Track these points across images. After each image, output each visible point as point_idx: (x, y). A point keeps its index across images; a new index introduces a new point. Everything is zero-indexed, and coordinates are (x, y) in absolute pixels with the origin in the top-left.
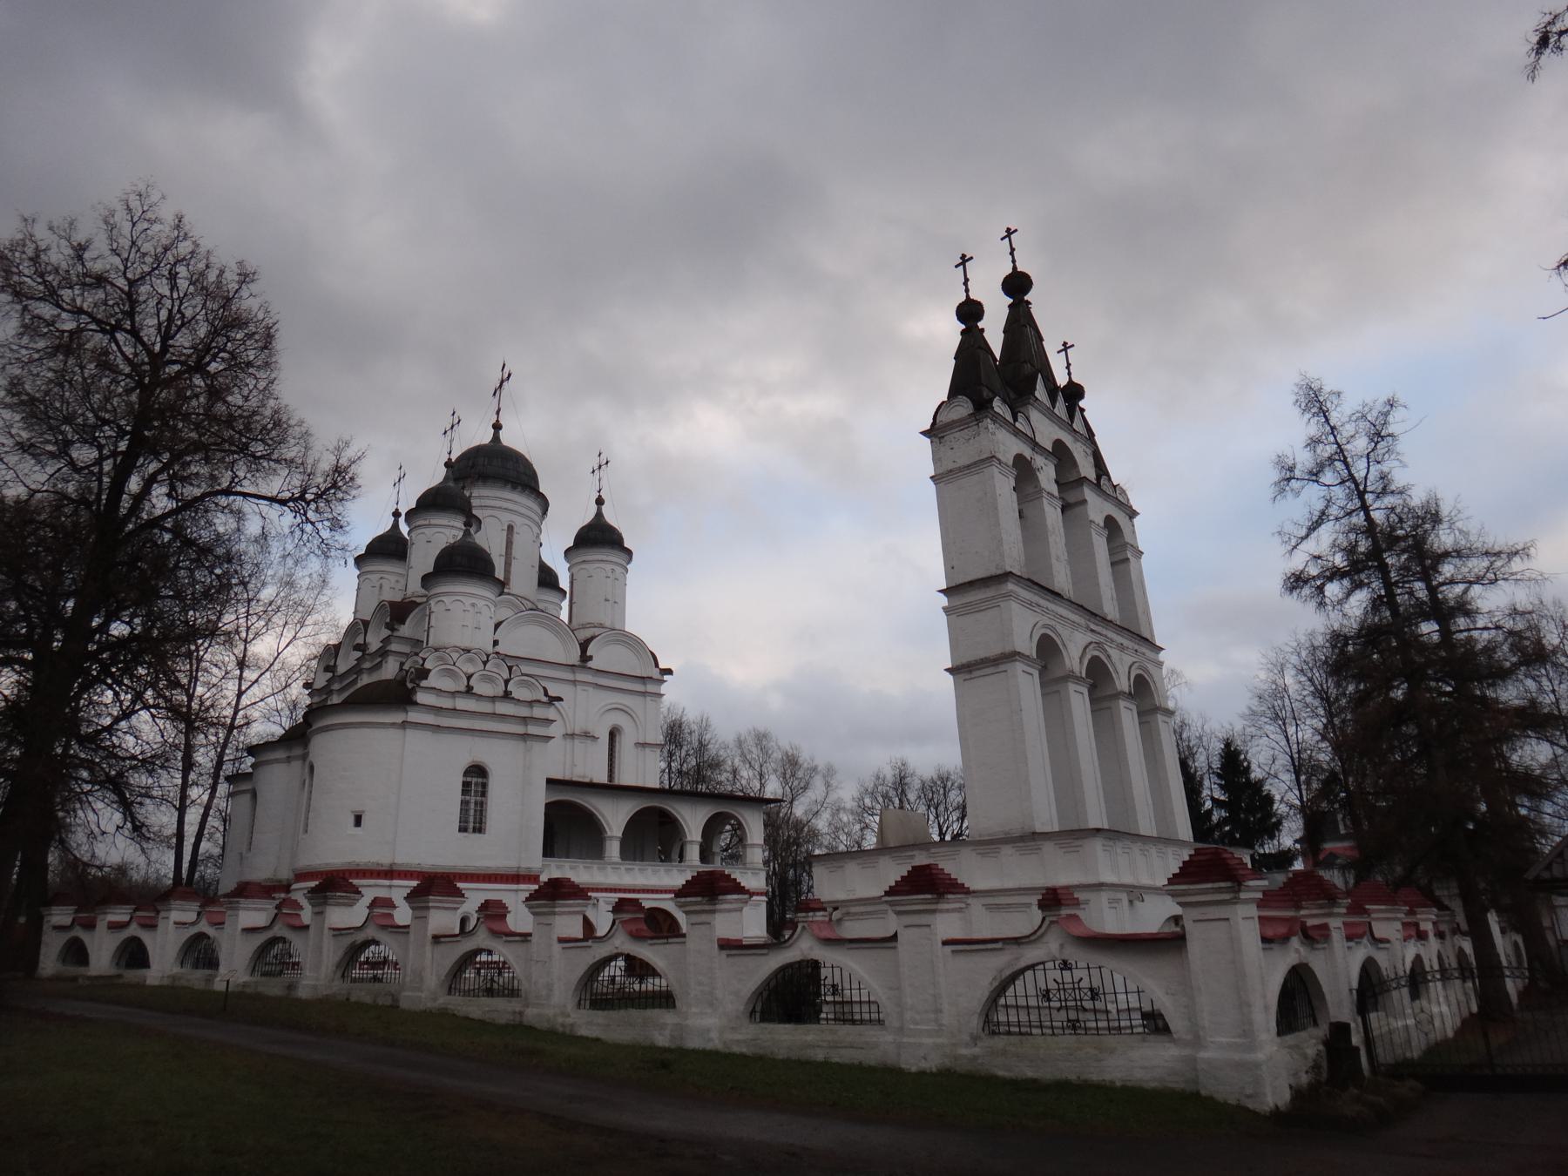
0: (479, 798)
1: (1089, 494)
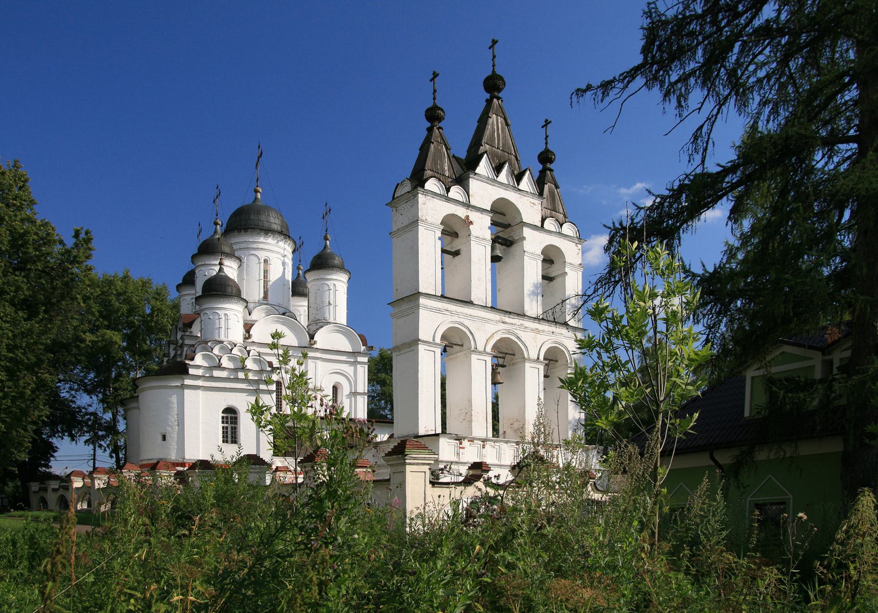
0: (233, 425)
1: (527, 232)
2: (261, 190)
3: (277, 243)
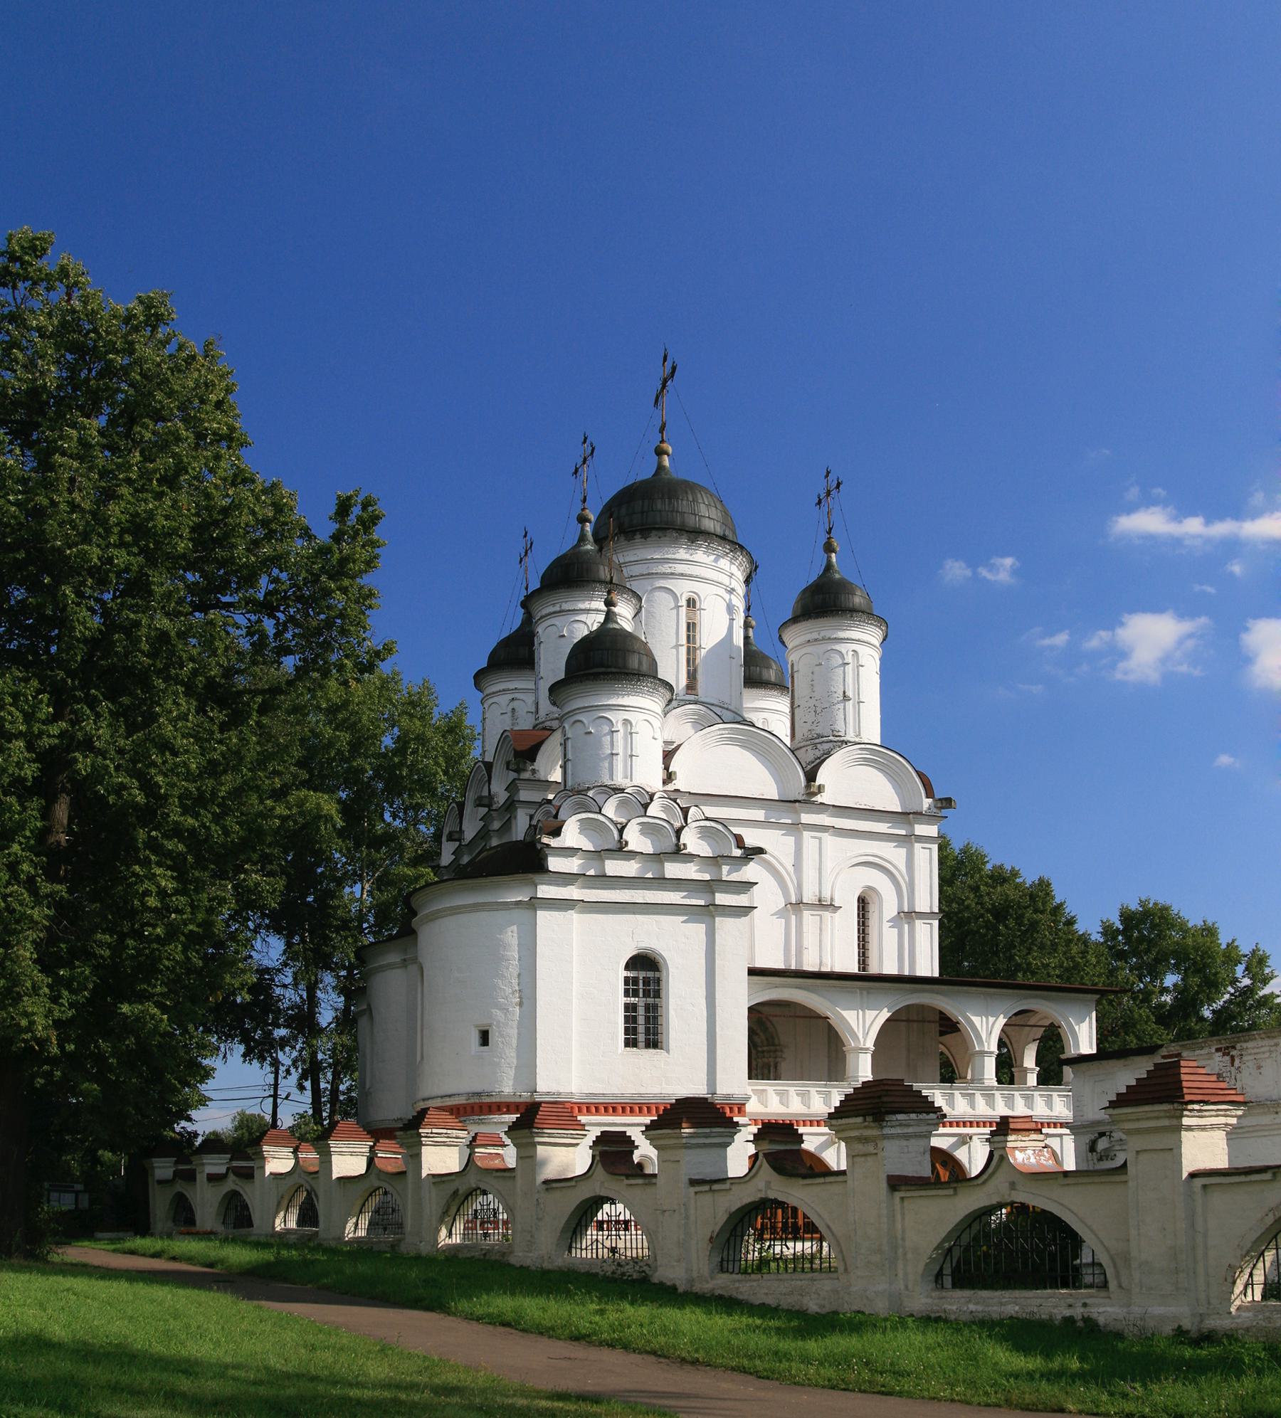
0: (650, 1000)
2: (670, 450)
3: (716, 561)
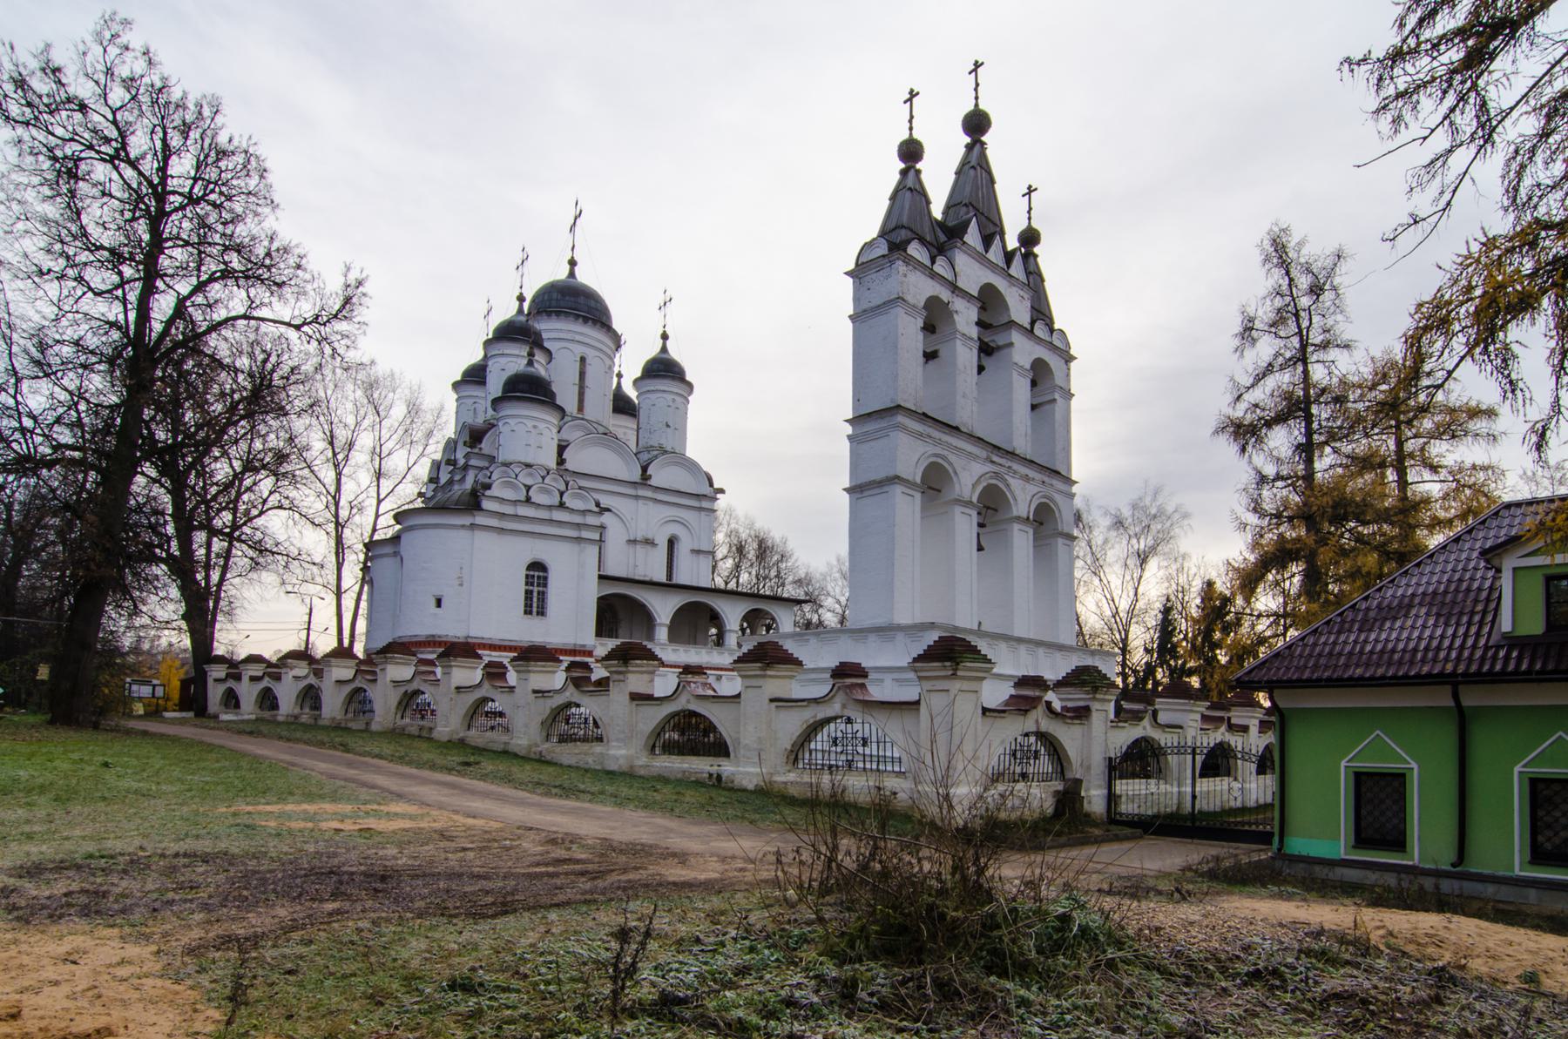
1: (1016, 337)
